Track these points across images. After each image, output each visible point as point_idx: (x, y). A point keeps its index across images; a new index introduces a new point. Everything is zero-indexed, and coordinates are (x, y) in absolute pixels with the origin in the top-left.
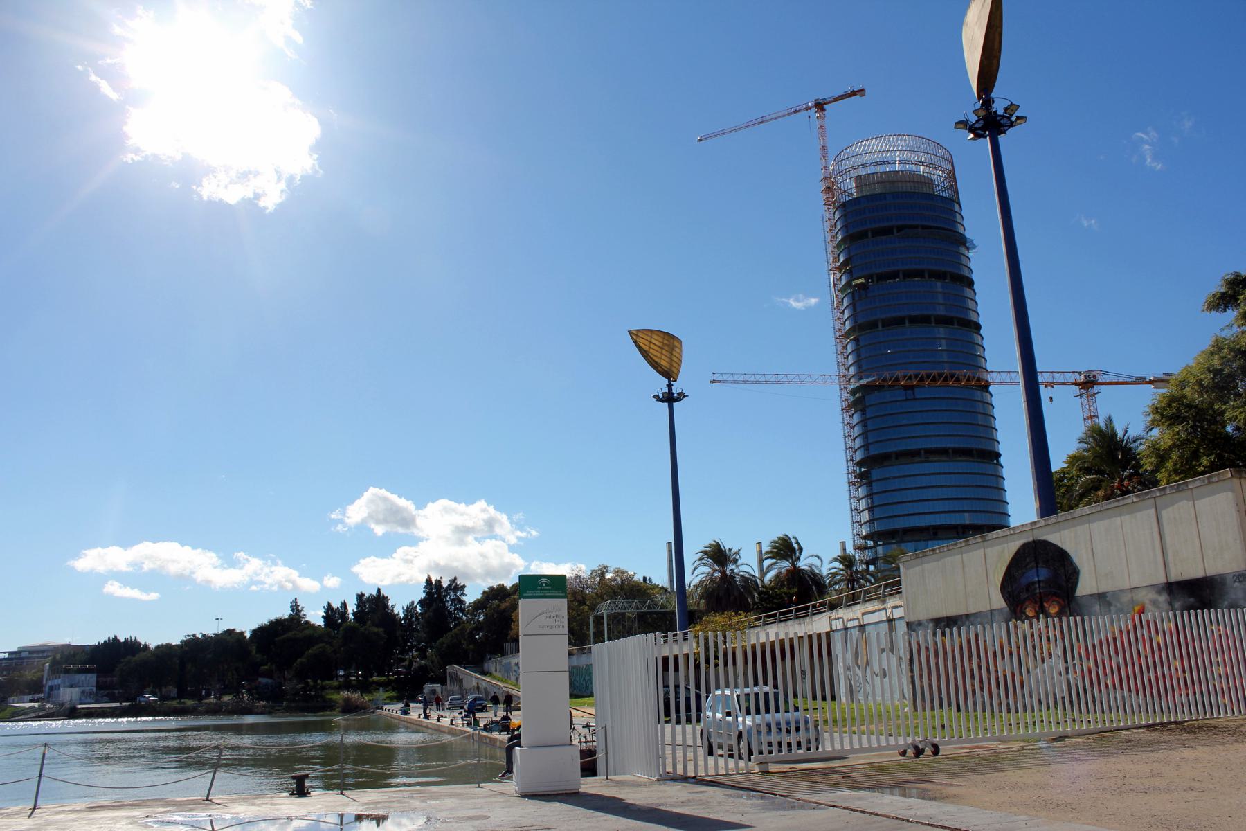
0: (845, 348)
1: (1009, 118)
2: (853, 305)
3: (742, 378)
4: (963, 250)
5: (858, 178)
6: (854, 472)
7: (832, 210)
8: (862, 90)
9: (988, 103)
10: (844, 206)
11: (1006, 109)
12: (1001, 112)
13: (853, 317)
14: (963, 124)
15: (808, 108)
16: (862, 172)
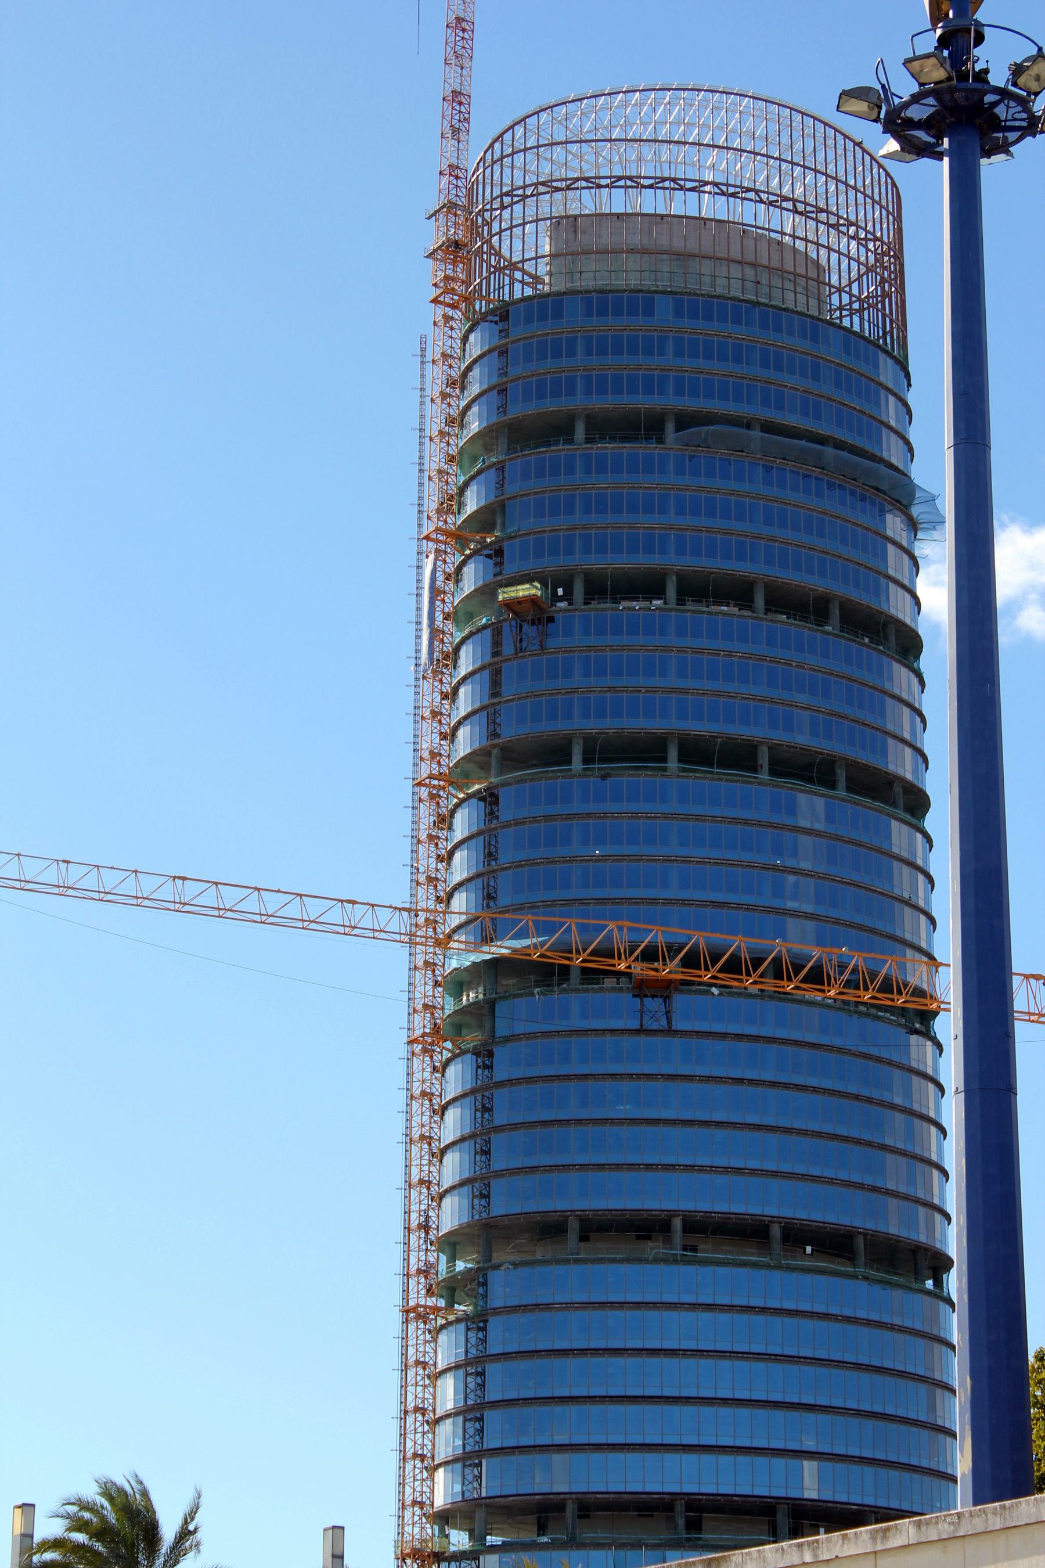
0: (445, 821)
1: (1024, 103)
3: (51, 876)
4: (894, 525)
5: (566, 225)
6: (425, 1272)
10: (502, 314)
12: (998, 78)
13: (488, 713)
16: (584, 202)
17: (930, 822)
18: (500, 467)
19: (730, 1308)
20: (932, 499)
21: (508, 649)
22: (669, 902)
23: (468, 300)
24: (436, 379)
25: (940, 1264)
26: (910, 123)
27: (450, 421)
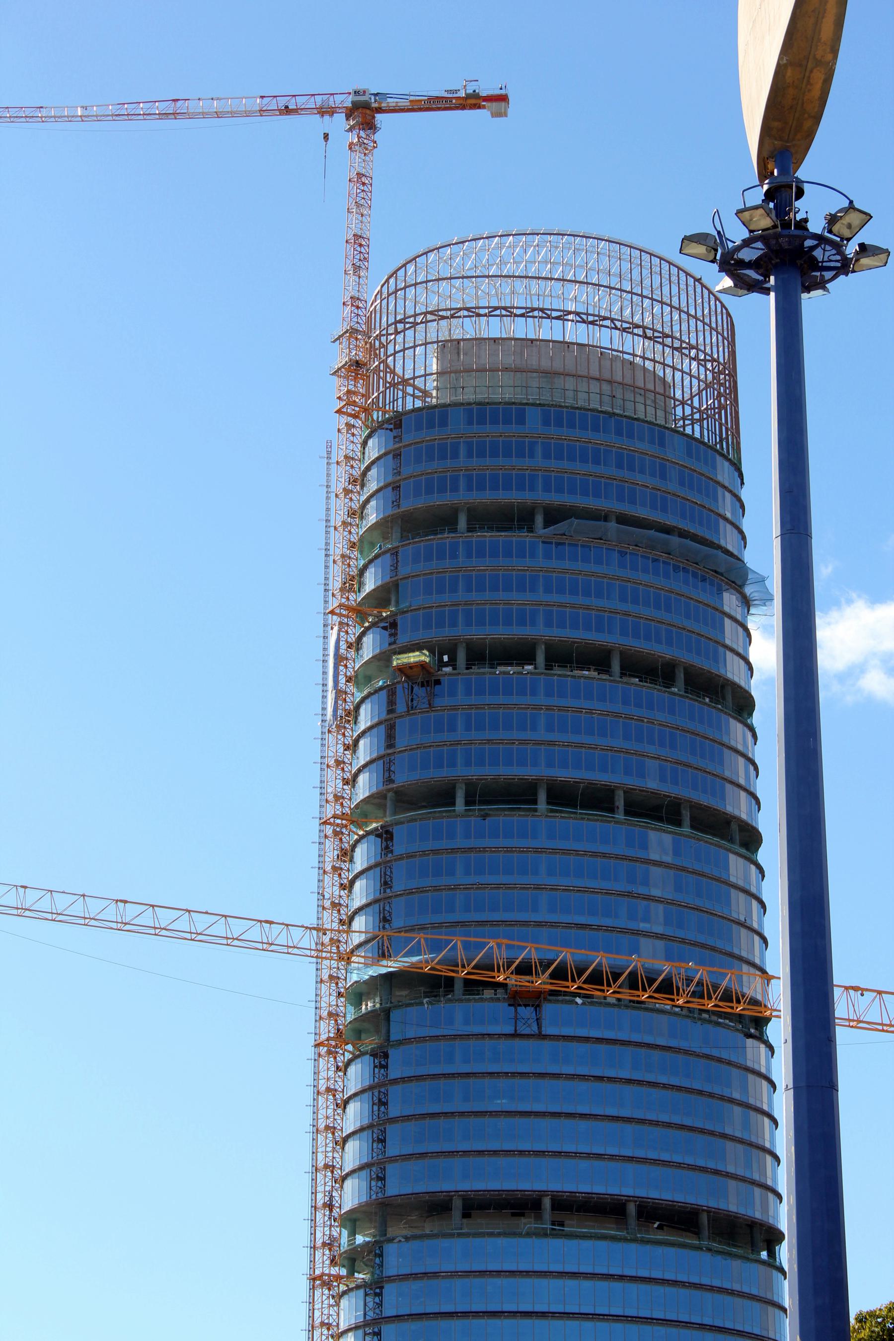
0: (347, 854)
1: (838, 248)
2: (388, 728)
4: (730, 602)
5: (450, 348)
6: (329, 1244)
7: (361, 433)
8: (503, 99)
9: (782, 193)
11: (832, 220)
12: (816, 226)
13: (384, 762)
14: (709, 244)
15: (325, 111)
16: (465, 329)
17: (762, 856)
18: (394, 552)
19: (593, 1276)
20: (762, 580)
21: (401, 707)
22: (539, 924)
23: (367, 410)
24: (340, 477)
25: (773, 1237)
26: (742, 264)
27: (352, 513)
